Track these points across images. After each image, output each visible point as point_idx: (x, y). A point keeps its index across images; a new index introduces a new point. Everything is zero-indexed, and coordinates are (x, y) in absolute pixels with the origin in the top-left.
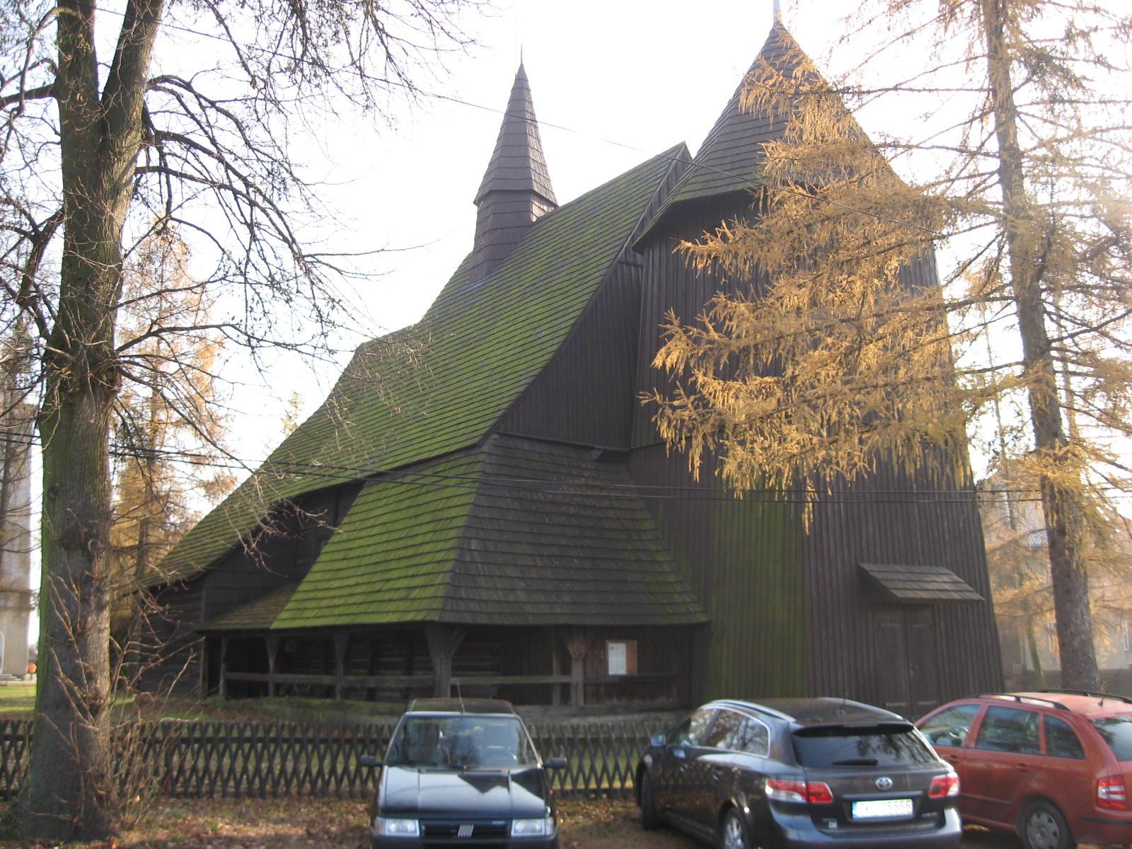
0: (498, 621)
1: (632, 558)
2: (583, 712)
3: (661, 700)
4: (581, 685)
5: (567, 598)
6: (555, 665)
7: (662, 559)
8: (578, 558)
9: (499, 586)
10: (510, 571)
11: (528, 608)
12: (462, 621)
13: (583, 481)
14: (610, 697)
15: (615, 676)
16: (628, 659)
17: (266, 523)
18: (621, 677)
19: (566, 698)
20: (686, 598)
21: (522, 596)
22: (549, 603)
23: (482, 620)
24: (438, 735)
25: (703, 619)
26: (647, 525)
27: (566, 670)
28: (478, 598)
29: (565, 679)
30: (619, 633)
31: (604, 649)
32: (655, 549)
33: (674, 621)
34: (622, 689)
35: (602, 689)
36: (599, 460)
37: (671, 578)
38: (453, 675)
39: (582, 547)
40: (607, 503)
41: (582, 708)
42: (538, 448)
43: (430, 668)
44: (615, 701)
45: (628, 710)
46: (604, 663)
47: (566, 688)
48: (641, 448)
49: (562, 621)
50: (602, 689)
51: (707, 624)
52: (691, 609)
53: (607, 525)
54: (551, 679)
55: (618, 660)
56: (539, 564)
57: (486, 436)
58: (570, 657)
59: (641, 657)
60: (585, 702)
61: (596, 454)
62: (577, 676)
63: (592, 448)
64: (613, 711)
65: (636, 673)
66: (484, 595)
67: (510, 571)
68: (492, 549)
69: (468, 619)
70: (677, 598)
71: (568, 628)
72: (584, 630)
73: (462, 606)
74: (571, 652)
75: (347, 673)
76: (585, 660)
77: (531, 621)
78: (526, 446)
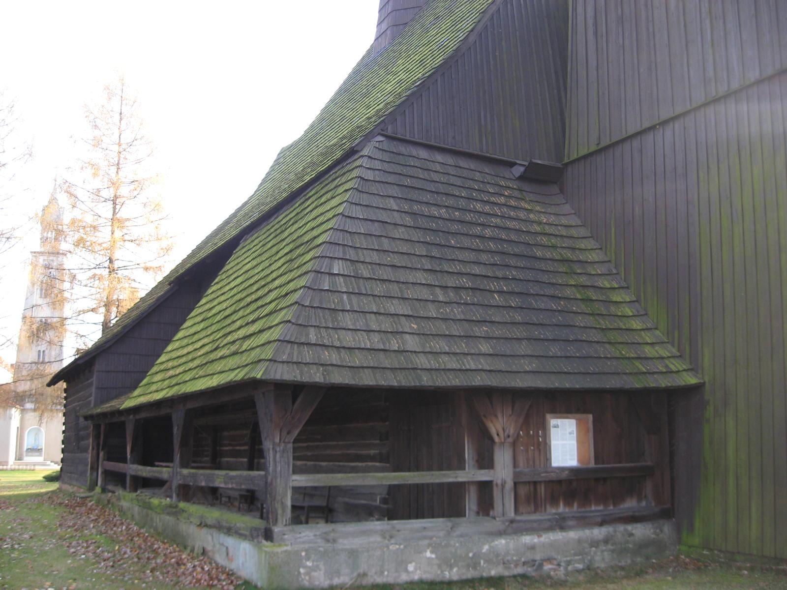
0: (367, 379)
1: (579, 296)
2: (514, 528)
3: (630, 504)
4: (510, 484)
5: (485, 347)
6: (469, 453)
7: (619, 299)
8: (500, 292)
9: (374, 327)
10: (394, 307)
11: (422, 361)
12: (306, 379)
13: (502, 200)
14: (554, 501)
15: (562, 469)
16: (579, 442)
17: (709, 563)
18: (572, 470)
19: (486, 506)
20: (664, 353)
21: (412, 343)
22: (455, 354)
23: (339, 378)
24: (533, 432)
25: (691, 380)
26: (594, 256)
27: (485, 461)
28: (338, 344)
29: (483, 476)
30: (564, 401)
31: (544, 427)
32: (608, 286)
33: (652, 382)
34: (573, 488)
35: (542, 490)
36: (522, 178)
37: (636, 324)
38: (295, 472)
39: (505, 278)
40: (538, 229)
41: (512, 521)
42: (439, 157)
43: (255, 457)
44: (561, 508)
45: (584, 522)
46: (543, 448)
47: (485, 487)
48: (578, 160)
49: (478, 381)
50: (542, 490)
51: (697, 388)
52: (672, 366)
53: (539, 254)
54: (461, 476)
55: (565, 444)
56: (441, 298)
57: (368, 137)
58: (491, 439)
59: (600, 439)
60: (516, 511)
61: (518, 171)
62: (503, 471)
63: (512, 165)
64: (560, 524)
65: (592, 465)
66: (349, 340)
67: (394, 307)
68: (366, 274)
69: (317, 376)
70: (649, 351)
71: (488, 393)
72: (513, 396)
73: (308, 355)
74: (493, 431)
75: (184, 465)
76: (514, 445)
77: (426, 381)
78: (423, 153)
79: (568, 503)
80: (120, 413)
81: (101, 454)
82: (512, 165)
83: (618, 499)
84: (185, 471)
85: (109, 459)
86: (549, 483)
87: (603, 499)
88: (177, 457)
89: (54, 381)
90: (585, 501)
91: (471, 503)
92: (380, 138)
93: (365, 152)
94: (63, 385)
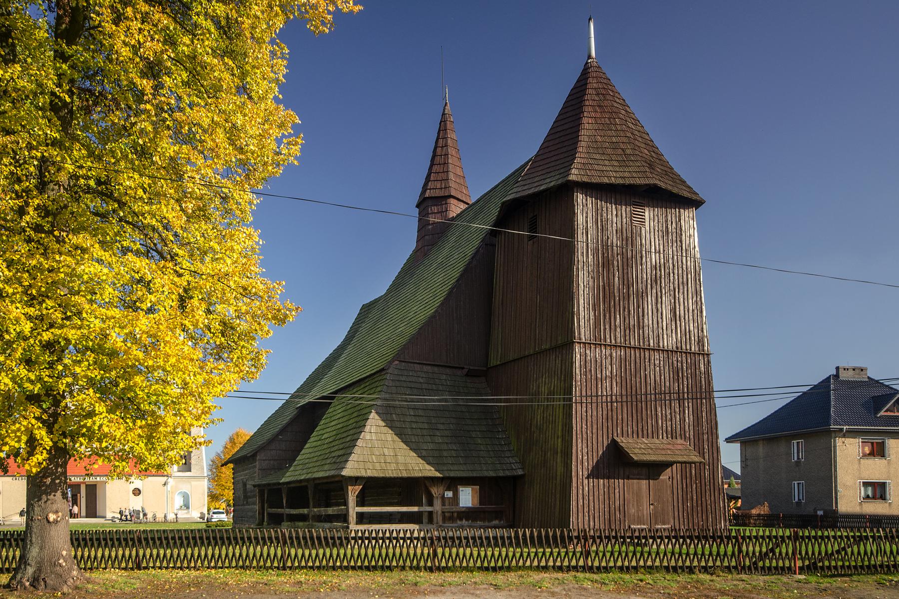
4: (440, 512)
14: (461, 520)
25: (520, 472)
27: (431, 504)
29: (429, 509)
30: (467, 481)
34: (469, 514)
47: (430, 513)
51: (522, 476)
55: (467, 497)
57: (391, 362)
59: (483, 498)
62: (437, 507)
75: (314, 507)
79: (466, 520)
80: (279, 484)
81: (266, 505)
82: (463, 368)
83: (490, 521)
84: (316, 510)
85: (271, 507)
86: (458, 512)
87: (483, 520)
88: (311, 504)
89: (225, 464)
90: (475, 519)
91: (425, 520)
92: (397, 362)
93: (390, 371)
94: (231, 466)
